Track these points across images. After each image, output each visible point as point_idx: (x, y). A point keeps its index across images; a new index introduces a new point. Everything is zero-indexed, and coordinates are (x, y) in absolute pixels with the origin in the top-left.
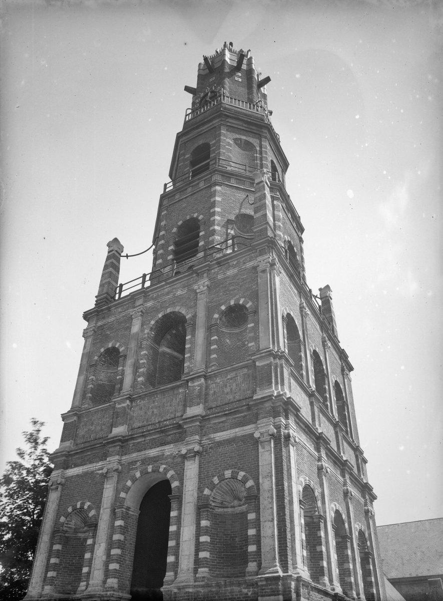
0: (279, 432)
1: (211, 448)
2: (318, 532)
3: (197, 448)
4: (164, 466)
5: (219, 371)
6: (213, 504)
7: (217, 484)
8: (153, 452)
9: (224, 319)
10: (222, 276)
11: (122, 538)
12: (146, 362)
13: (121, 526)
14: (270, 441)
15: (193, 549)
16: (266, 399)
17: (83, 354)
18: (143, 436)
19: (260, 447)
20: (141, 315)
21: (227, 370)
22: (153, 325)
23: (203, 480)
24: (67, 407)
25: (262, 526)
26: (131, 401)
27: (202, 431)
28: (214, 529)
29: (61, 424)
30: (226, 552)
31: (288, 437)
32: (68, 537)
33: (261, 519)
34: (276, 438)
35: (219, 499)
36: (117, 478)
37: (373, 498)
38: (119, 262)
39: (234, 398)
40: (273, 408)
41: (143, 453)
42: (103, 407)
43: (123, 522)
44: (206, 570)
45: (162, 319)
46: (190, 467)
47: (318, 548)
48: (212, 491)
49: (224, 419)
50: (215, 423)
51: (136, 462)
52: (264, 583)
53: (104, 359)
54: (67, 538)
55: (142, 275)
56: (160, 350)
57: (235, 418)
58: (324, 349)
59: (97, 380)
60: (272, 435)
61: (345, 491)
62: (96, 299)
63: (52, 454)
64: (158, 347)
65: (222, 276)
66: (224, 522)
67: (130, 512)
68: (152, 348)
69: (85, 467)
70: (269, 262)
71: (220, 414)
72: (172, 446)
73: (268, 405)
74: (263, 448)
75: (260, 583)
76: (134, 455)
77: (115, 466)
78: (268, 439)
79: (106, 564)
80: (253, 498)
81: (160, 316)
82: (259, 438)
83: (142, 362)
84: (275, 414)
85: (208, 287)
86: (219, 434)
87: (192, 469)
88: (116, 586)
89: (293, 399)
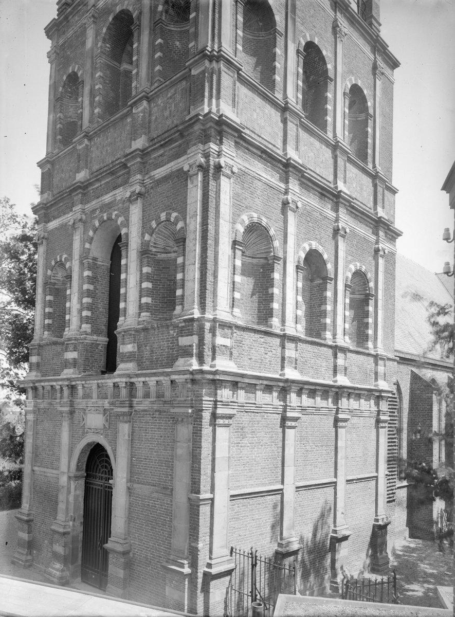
0: (208, 162)
2: (272, 274)
3: (138, 188)
5: (160, 88)
6: (154, 250)
7: (156, 228)
8: (107, 198)
9: (171, 11)
11: (91, 287)
12: (101, 87)
13: (88, 276)
14: (197, 174)
16: (193, 121)
19: (189, 181)
22: (105, 34)
23: (145, 228)
24: (42, 155)
25: (186, 269)
26: (90, 140)
27: (144, 169)
28: (156, 275)
29: (38, 172)
30: (170, 297)
31: (218, 168)
33: (186, 263)
34: (204, 169)
35: (161, 244)
36: (83, 228)
37: (393, 235)
39: (173, 122)
40: (204, 131)
41: (100, 199)
42: (69, 150)
43: (91, 272)
44: (148, 314)
48: (151, 235)
49: (161, 152)
50: (155, 158)
53: (70, 90)
54: (57, 289)
56: (122, 68)
57: (171, 149)
58: (336, 38)
59: (66, 117)
60: (200, 166)
61: (336, 228)
64: (118, 65)
66: (168, 268)
67: (99, 263)
69: (60, 219)
71: (157, 146)
73: (197, 127)
74: (192, 183)
75: (180, 325)
76: (94, 202)
77: (78, 216)
81: (111, 19)
82: (189, 171)
83: (97, 87)
84: (205, 138)
87: (136, 212)
88: (89, 331)
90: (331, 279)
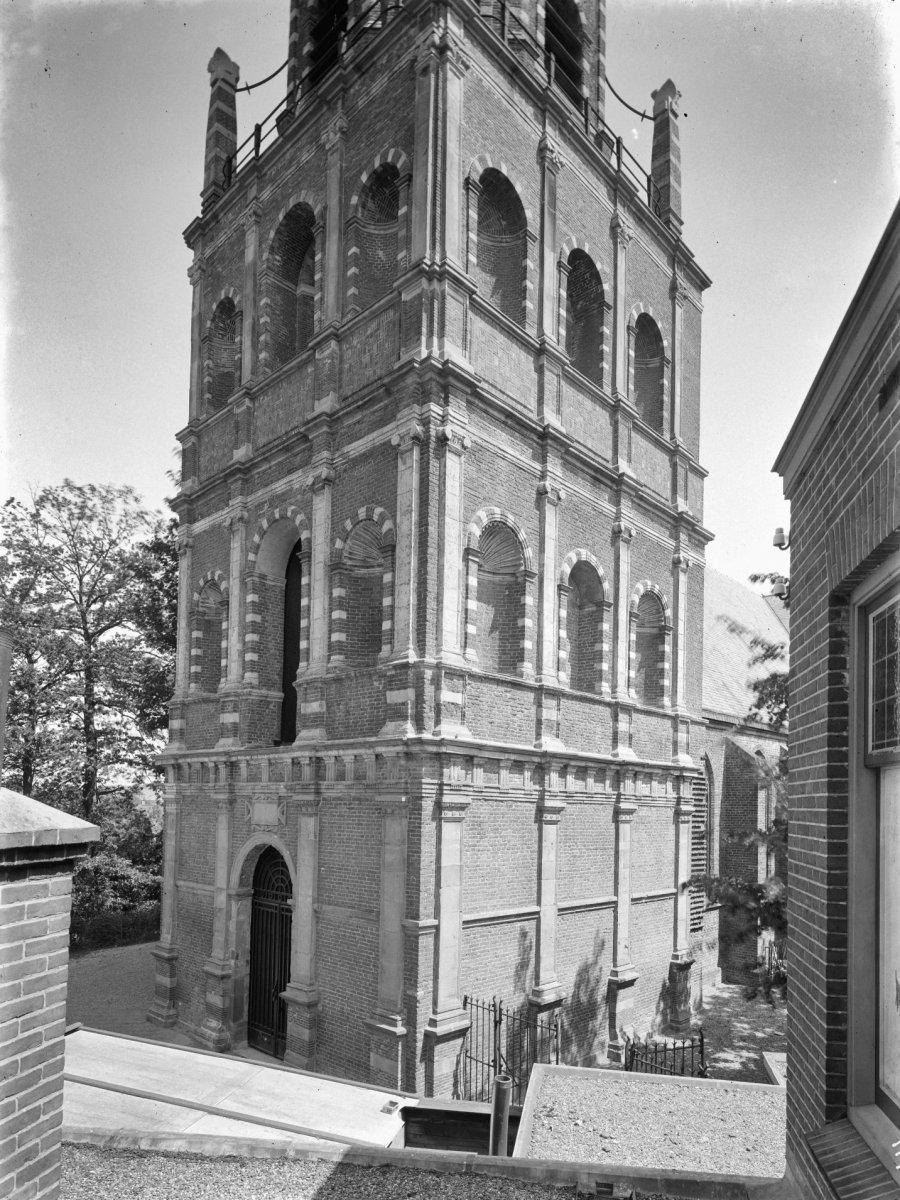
0: (427, 431)
1: (345, 471)
3: (324, 472)
4: (293, 507)
6: (349, 563)
7: (351, 531)
8: (280, 486)
9: (370, 204)
10: (365, 98)
11: (258, 619)
14: (412, 449)
15: (326, 629)
17: (193, 319)
18: (265, 459)
20: (257, 222)
21: (365, 318)
23: (336, 530)
26: (253, 399)
27: (334, 442)
32: (209, 621)
34: (421, 442)
35: (360, 553)
38: (233, 107)
40: (421, 384)
43: (257, 596)
44: (342, 657)
45: (286, 225)
46: (320, 506)
47: (660, 648)
49: (358, 417)
51: (263, 504)
52: (393, 672)
54: (209, 621)
55: (253, 130)
56: (298, 292)
58: (615, 244)
60: (416, 438)
62: (202, 200)
63: (175, 500)
64: (293, 287)
65: (365, 98)
68: (280, 290)
69: (211, 518)
70: (433, 45)
72: (300, 472)
73: (411, 380)
74: (405, 463)
75: (389, 674)
78: (410, 447)
79: (242, 653)
80: (389, 549)
81: (281, 217)
82: (399, 445)
83: (262, 321)
84: (423, 397)
85: (343, 133)
86: (355, 445)
87: (322, 506)
88: (255, 682)
89: (453, 364)
90: (609, 605)
